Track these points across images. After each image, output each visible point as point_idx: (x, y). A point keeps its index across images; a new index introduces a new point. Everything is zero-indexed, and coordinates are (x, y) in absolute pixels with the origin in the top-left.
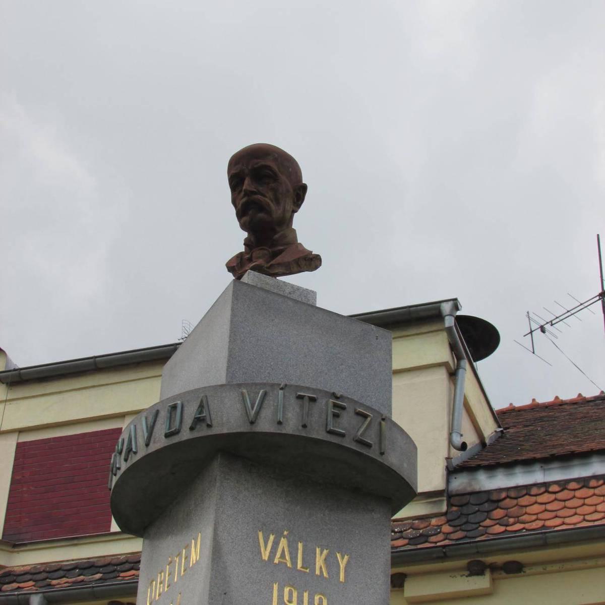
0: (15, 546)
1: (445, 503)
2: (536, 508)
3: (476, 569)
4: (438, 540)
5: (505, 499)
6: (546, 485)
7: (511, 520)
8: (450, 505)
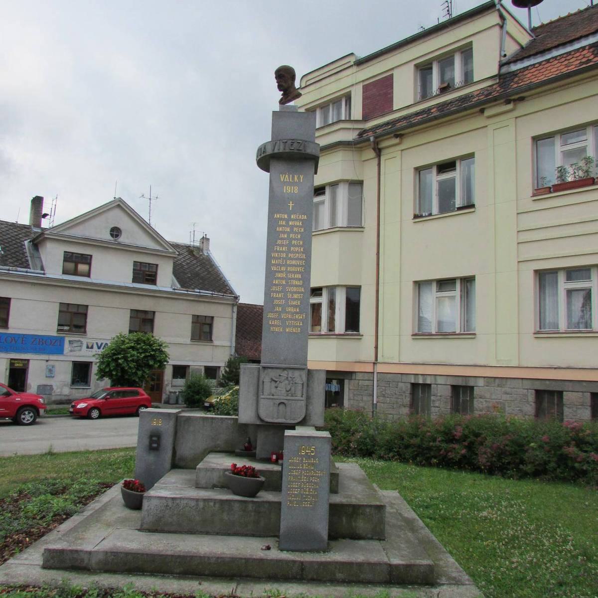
0: (366, 121)
2: (529, 75)
3: (508, 102)
4: (495, 94)
5: (519, 73)
7: (520, 81)
8: (500, 79)
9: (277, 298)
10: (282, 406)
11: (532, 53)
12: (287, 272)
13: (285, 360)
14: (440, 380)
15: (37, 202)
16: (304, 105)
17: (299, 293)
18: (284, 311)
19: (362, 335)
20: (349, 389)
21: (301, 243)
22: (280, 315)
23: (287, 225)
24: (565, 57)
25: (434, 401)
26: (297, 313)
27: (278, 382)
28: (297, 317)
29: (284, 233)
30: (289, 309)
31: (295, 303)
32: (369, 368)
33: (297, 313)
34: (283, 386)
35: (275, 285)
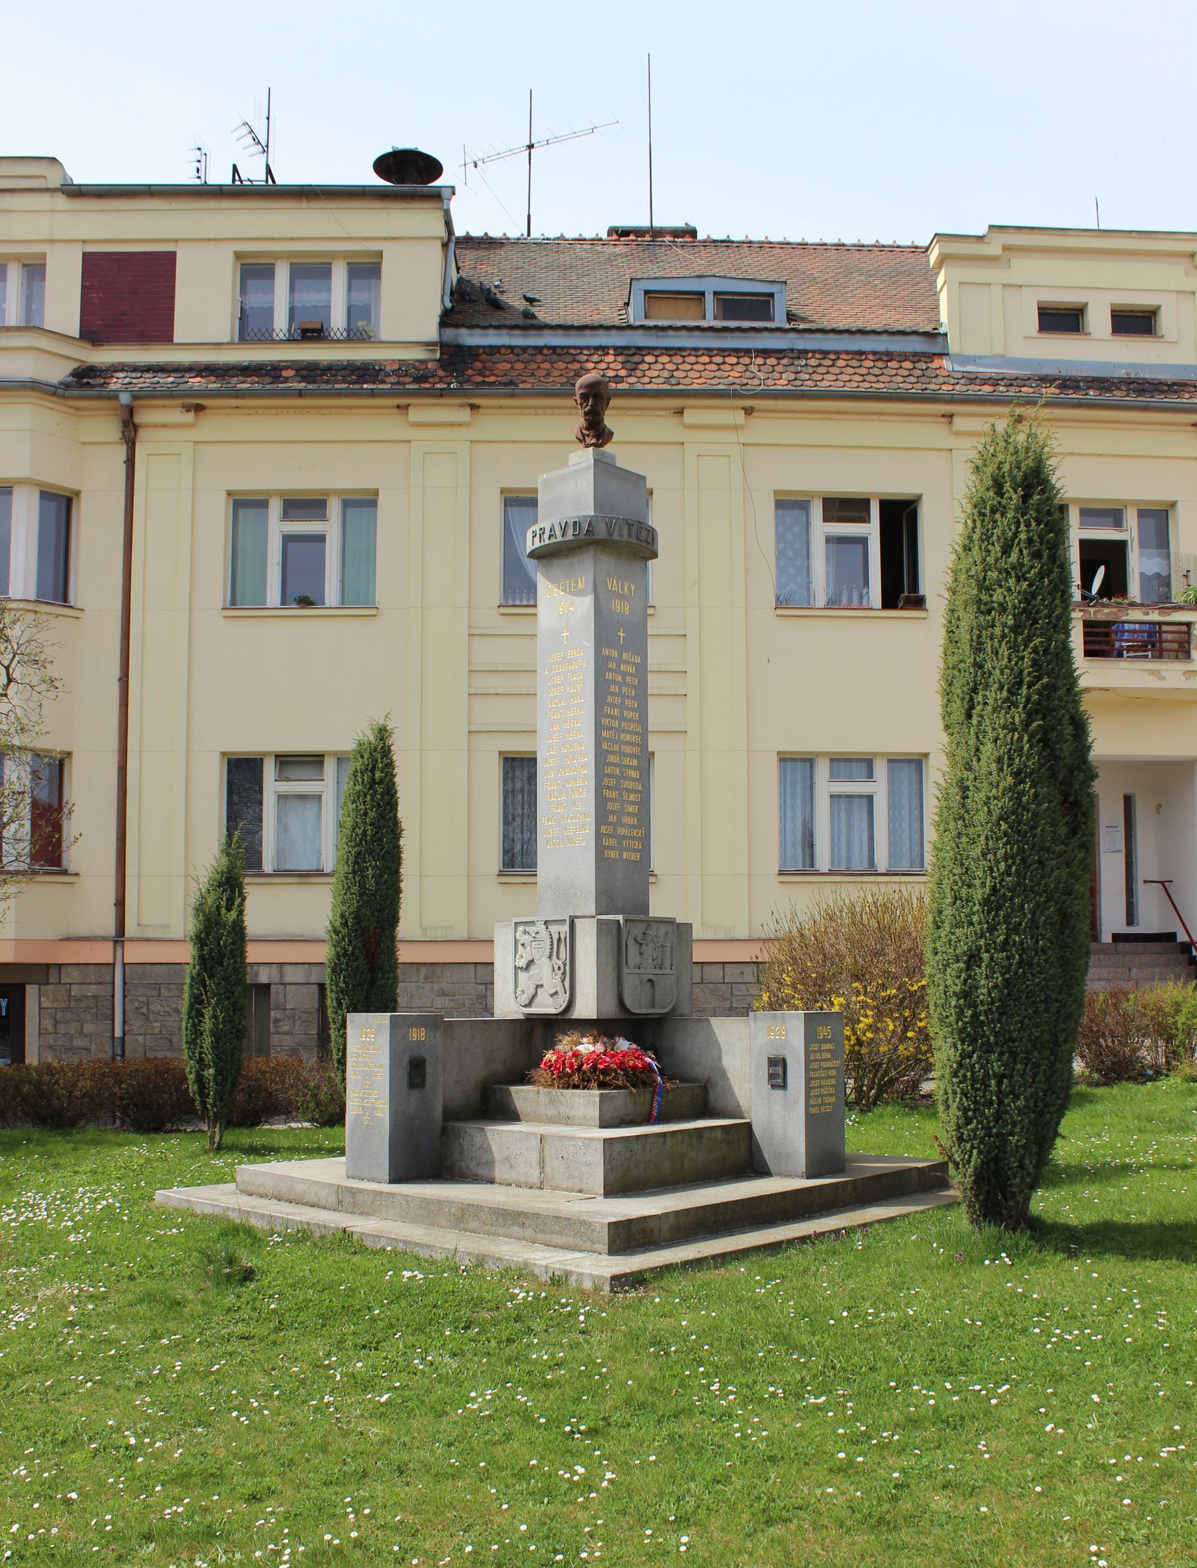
1: (439, 352)
6: (512, 348)
8: (442, 353)
11: (507, 323)
14: (292, 975)
19: (77, 874)
20: (40, 1008)
23: (618, 671)
24: (854, 368)
25: (277, 1021)
26: (635, 827)
32: (103, 953)
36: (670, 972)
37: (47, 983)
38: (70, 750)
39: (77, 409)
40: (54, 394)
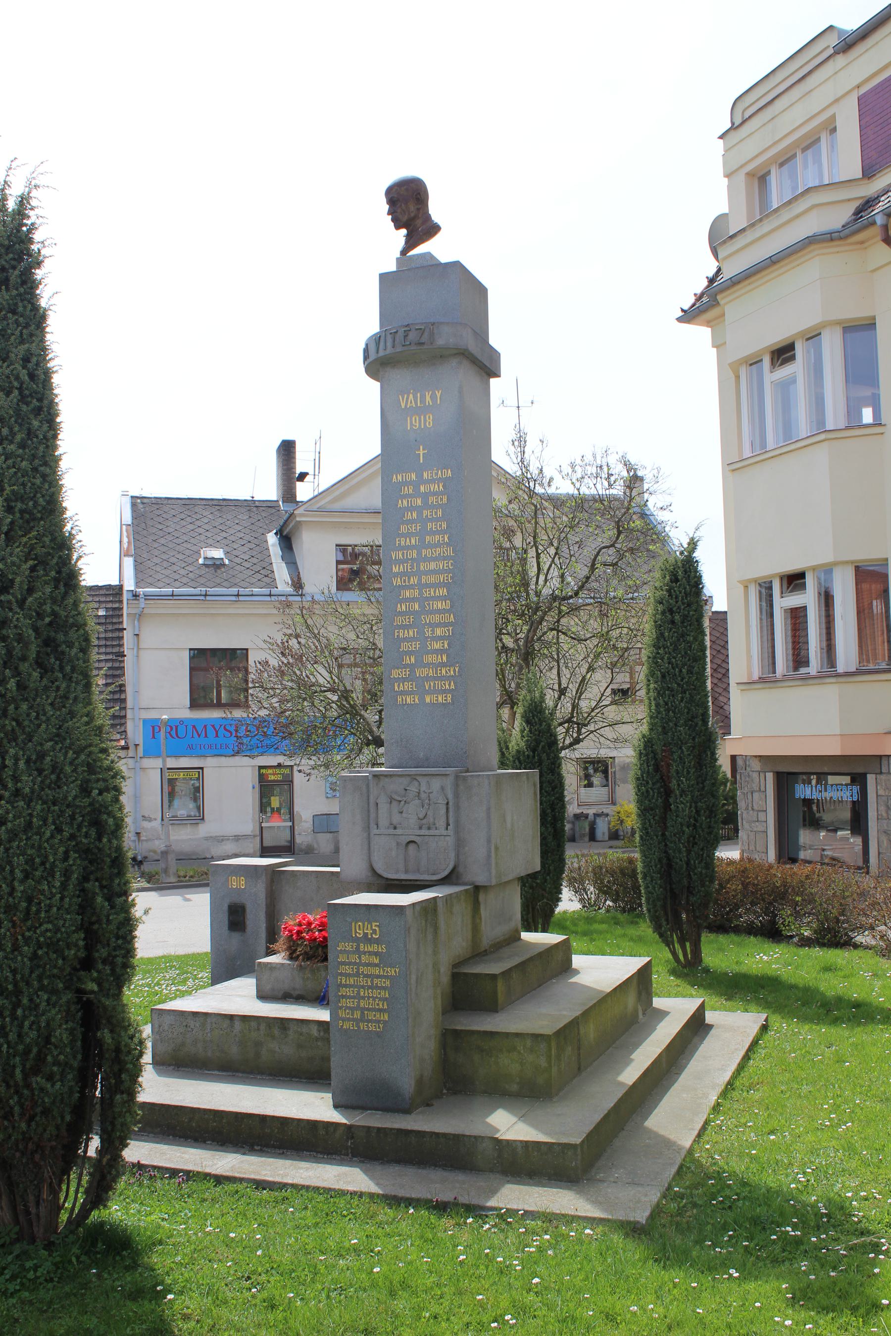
0: (869, 178)
9: (405, 639)
10: (412, 847)
12: (421, 586)
13: (427, 760)
15: (287, 450)
16: (742, 166)
17: (445, 625)
18: (420, 664)
20: (877, 796)
21: (444, 525)
22: (412, 671)
23: (417, 494)
26: (443, 665)
27: (402, 803)
28: (444, 672)
29: (411, 509)
30: (429, 659)
31: (437, 646)
33: (443, 665)
34: (413, 811)
35: (401, 614)
36: (445, 833)
37: (881, 773)
38: (885, 556)
39: (862, 243)
40: (832, 240)
